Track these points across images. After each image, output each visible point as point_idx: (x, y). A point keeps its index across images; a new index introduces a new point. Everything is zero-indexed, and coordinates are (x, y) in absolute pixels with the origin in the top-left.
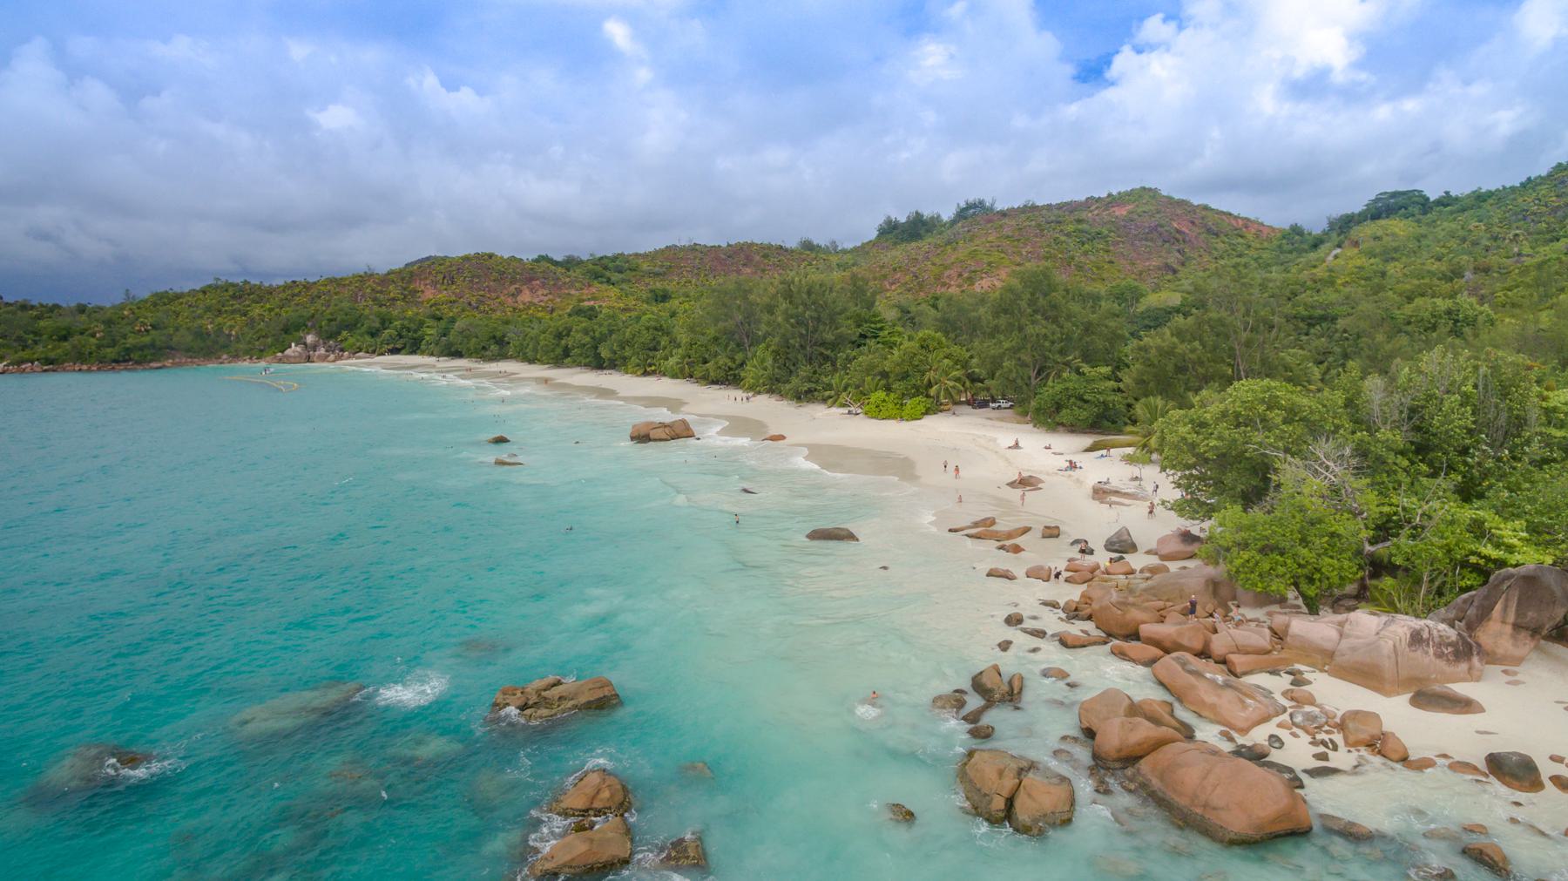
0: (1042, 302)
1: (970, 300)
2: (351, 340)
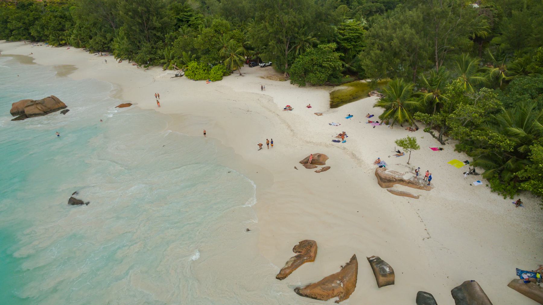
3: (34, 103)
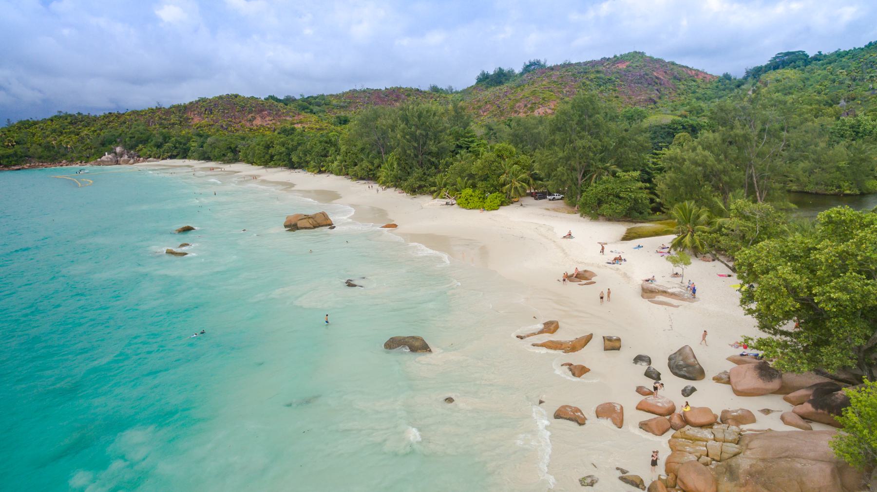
0: (588, 121)
1: (533, 121)
2: (145, 150)
3: (308, 217)
